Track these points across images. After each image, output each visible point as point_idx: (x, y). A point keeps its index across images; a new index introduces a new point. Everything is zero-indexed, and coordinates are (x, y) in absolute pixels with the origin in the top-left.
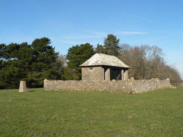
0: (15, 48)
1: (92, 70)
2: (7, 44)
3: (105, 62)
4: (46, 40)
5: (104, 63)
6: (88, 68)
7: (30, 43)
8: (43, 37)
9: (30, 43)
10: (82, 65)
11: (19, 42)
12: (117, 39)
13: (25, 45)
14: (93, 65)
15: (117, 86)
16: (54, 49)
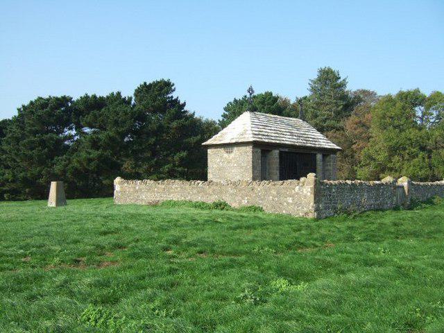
0: (93, 105)
1: (232, 155)
2: (76, 97)
3: (266, 134)
4: (166, 86)
5: (260, 136)
6: (222, 150)
7: (128, 92)
8: (34, 99)
9: (128, 92)
10: (209, 142)
11: (103, 92)
12: (341, 80)
13: (116, 99)
14: (234, 141)
15: (274, 196)
16: (184, 105)
